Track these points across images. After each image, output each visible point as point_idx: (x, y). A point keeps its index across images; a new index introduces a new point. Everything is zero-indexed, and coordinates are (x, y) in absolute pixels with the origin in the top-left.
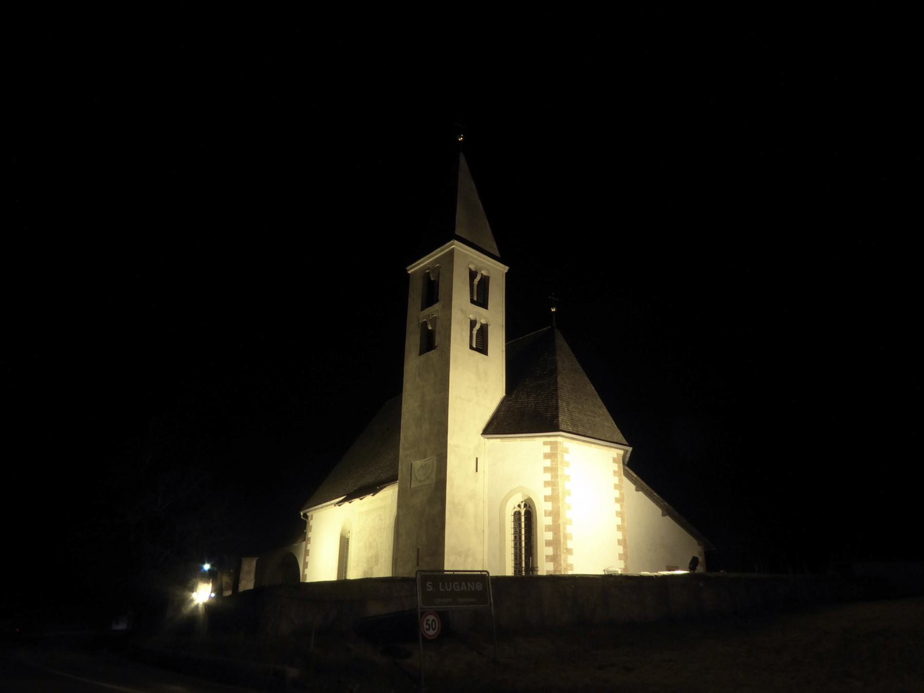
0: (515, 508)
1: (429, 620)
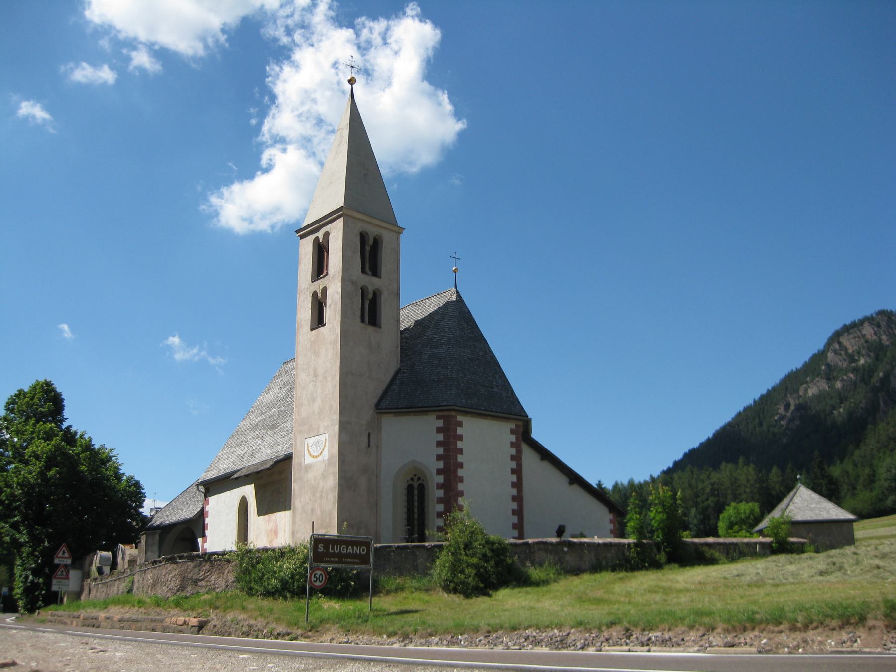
0: (408, 481)
1: (317, 574)
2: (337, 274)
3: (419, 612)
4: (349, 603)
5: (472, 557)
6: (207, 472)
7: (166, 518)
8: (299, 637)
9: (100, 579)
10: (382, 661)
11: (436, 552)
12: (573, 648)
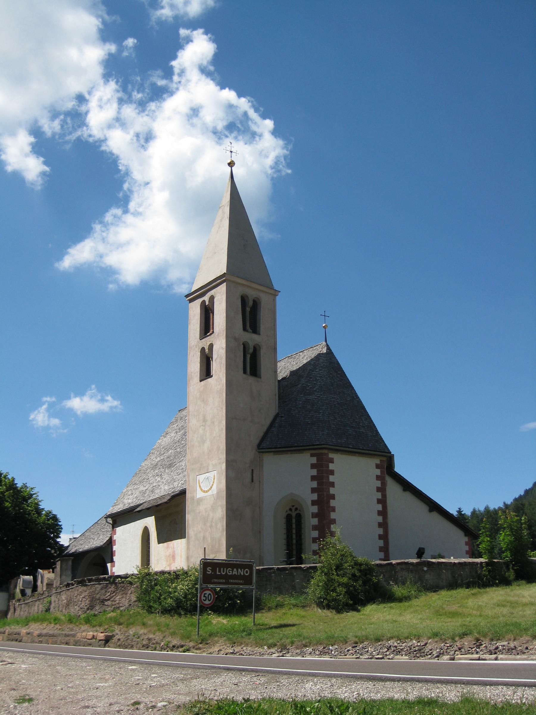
0: (287, 511)
2: (222, 333)
3: (296, 626)
4: (235, 619)
5: (343, 577)
6: (114, 506)
7: (80, 547)
8: (192, 649)
9: (23, 600)
10: (253, 671)
11: (311, 573)
12: (430, 656)
